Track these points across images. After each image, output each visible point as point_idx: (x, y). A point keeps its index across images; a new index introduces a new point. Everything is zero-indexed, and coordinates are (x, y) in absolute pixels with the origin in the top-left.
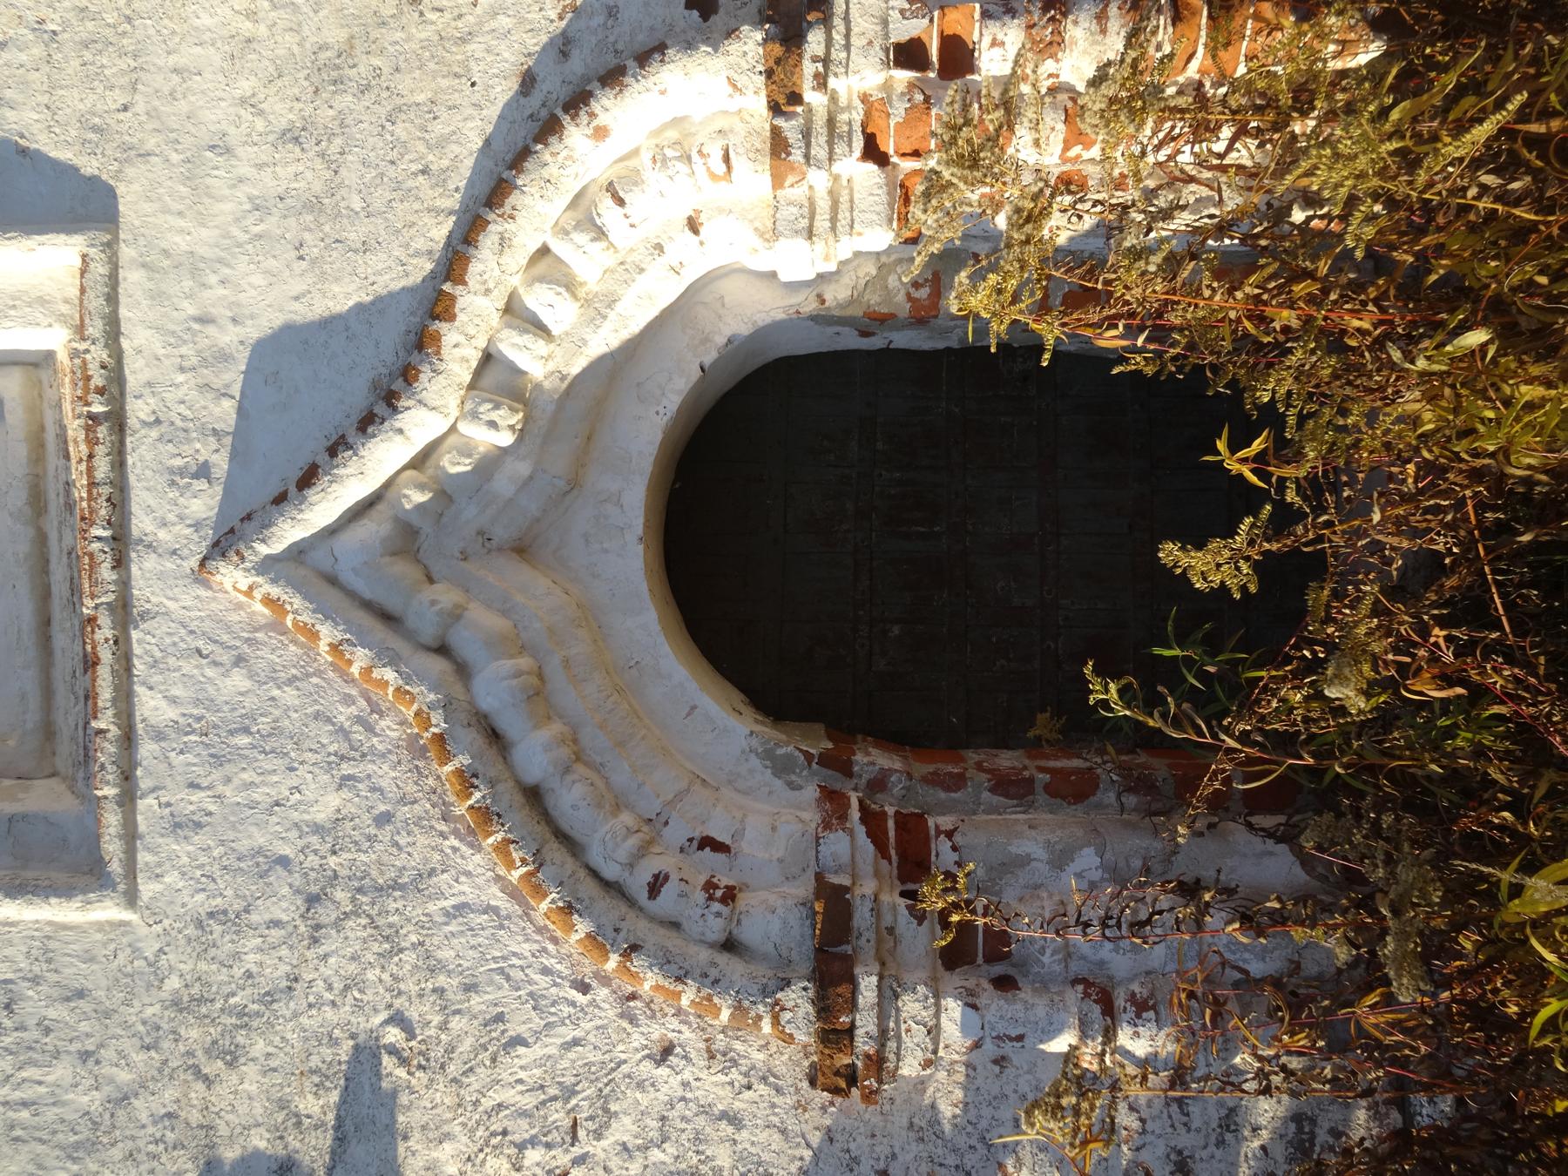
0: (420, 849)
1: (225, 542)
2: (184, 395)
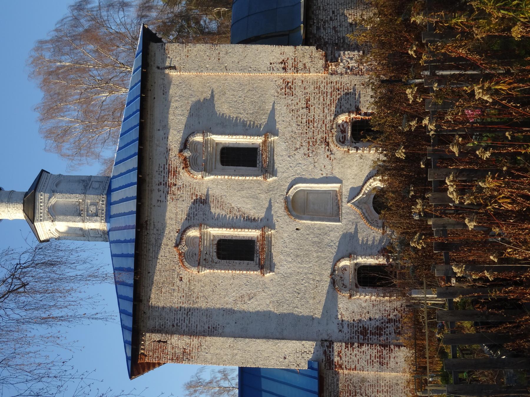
0: (359, 220)
1: (348, 202)
2: (346, 192)
